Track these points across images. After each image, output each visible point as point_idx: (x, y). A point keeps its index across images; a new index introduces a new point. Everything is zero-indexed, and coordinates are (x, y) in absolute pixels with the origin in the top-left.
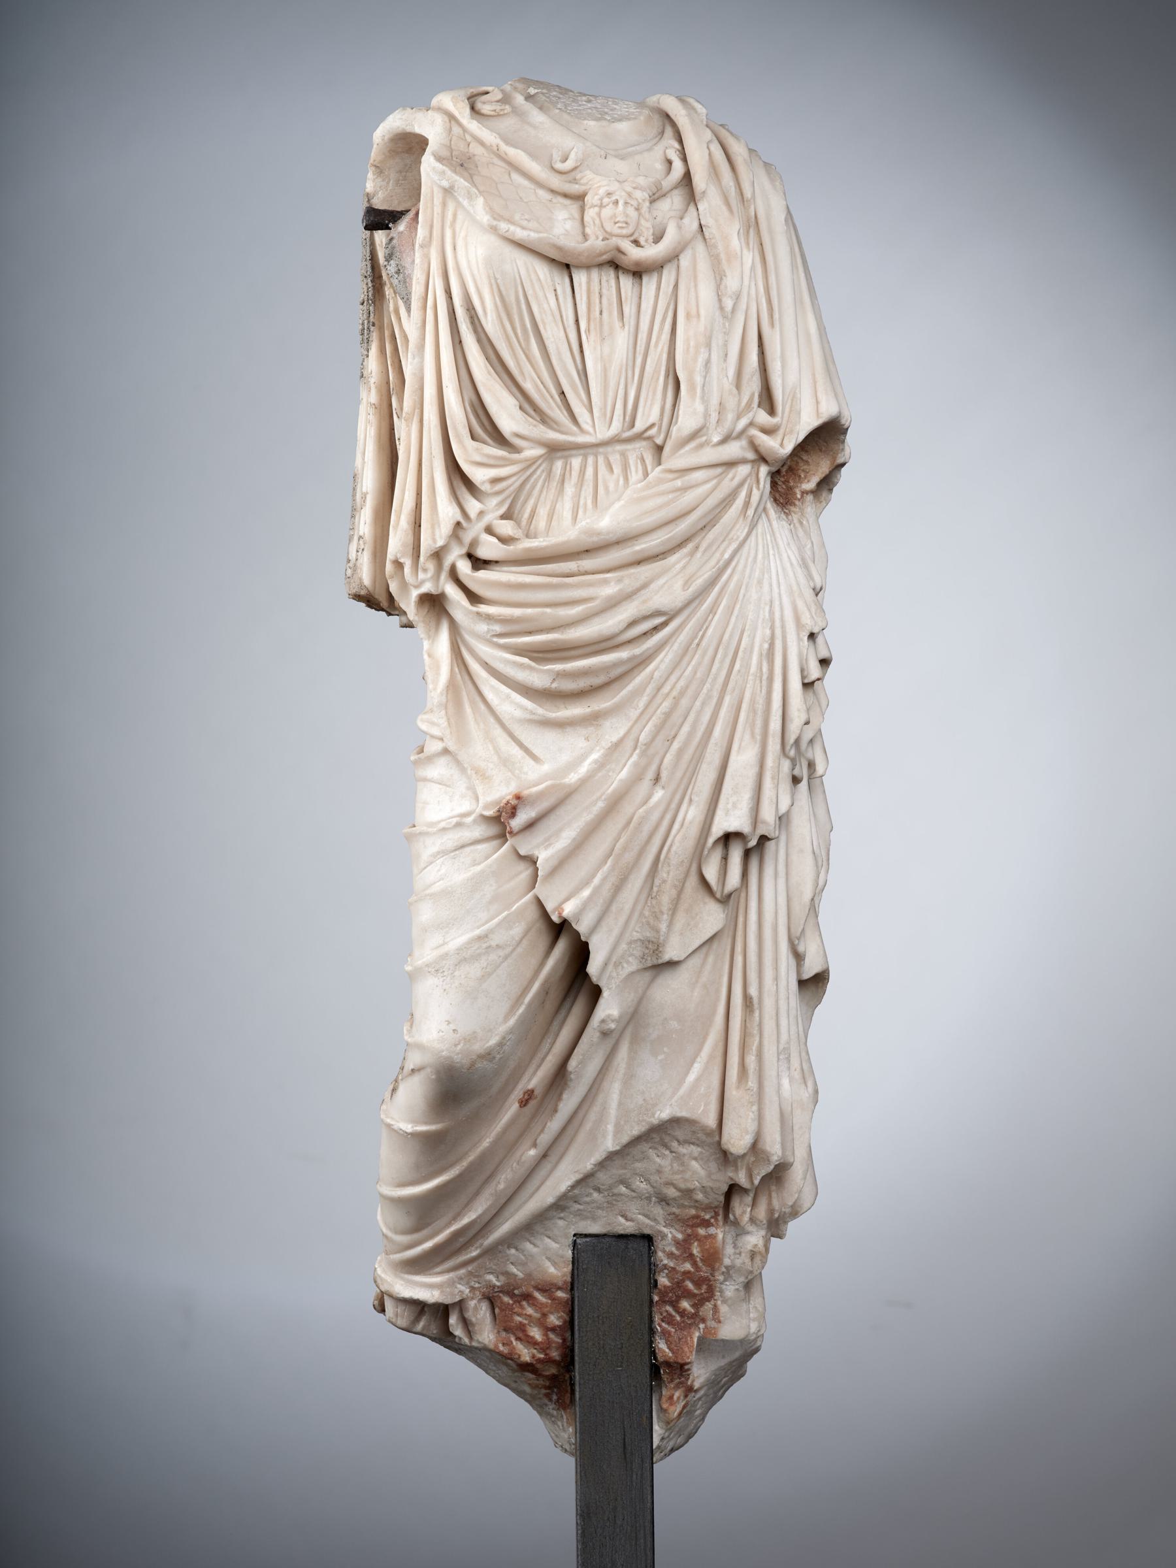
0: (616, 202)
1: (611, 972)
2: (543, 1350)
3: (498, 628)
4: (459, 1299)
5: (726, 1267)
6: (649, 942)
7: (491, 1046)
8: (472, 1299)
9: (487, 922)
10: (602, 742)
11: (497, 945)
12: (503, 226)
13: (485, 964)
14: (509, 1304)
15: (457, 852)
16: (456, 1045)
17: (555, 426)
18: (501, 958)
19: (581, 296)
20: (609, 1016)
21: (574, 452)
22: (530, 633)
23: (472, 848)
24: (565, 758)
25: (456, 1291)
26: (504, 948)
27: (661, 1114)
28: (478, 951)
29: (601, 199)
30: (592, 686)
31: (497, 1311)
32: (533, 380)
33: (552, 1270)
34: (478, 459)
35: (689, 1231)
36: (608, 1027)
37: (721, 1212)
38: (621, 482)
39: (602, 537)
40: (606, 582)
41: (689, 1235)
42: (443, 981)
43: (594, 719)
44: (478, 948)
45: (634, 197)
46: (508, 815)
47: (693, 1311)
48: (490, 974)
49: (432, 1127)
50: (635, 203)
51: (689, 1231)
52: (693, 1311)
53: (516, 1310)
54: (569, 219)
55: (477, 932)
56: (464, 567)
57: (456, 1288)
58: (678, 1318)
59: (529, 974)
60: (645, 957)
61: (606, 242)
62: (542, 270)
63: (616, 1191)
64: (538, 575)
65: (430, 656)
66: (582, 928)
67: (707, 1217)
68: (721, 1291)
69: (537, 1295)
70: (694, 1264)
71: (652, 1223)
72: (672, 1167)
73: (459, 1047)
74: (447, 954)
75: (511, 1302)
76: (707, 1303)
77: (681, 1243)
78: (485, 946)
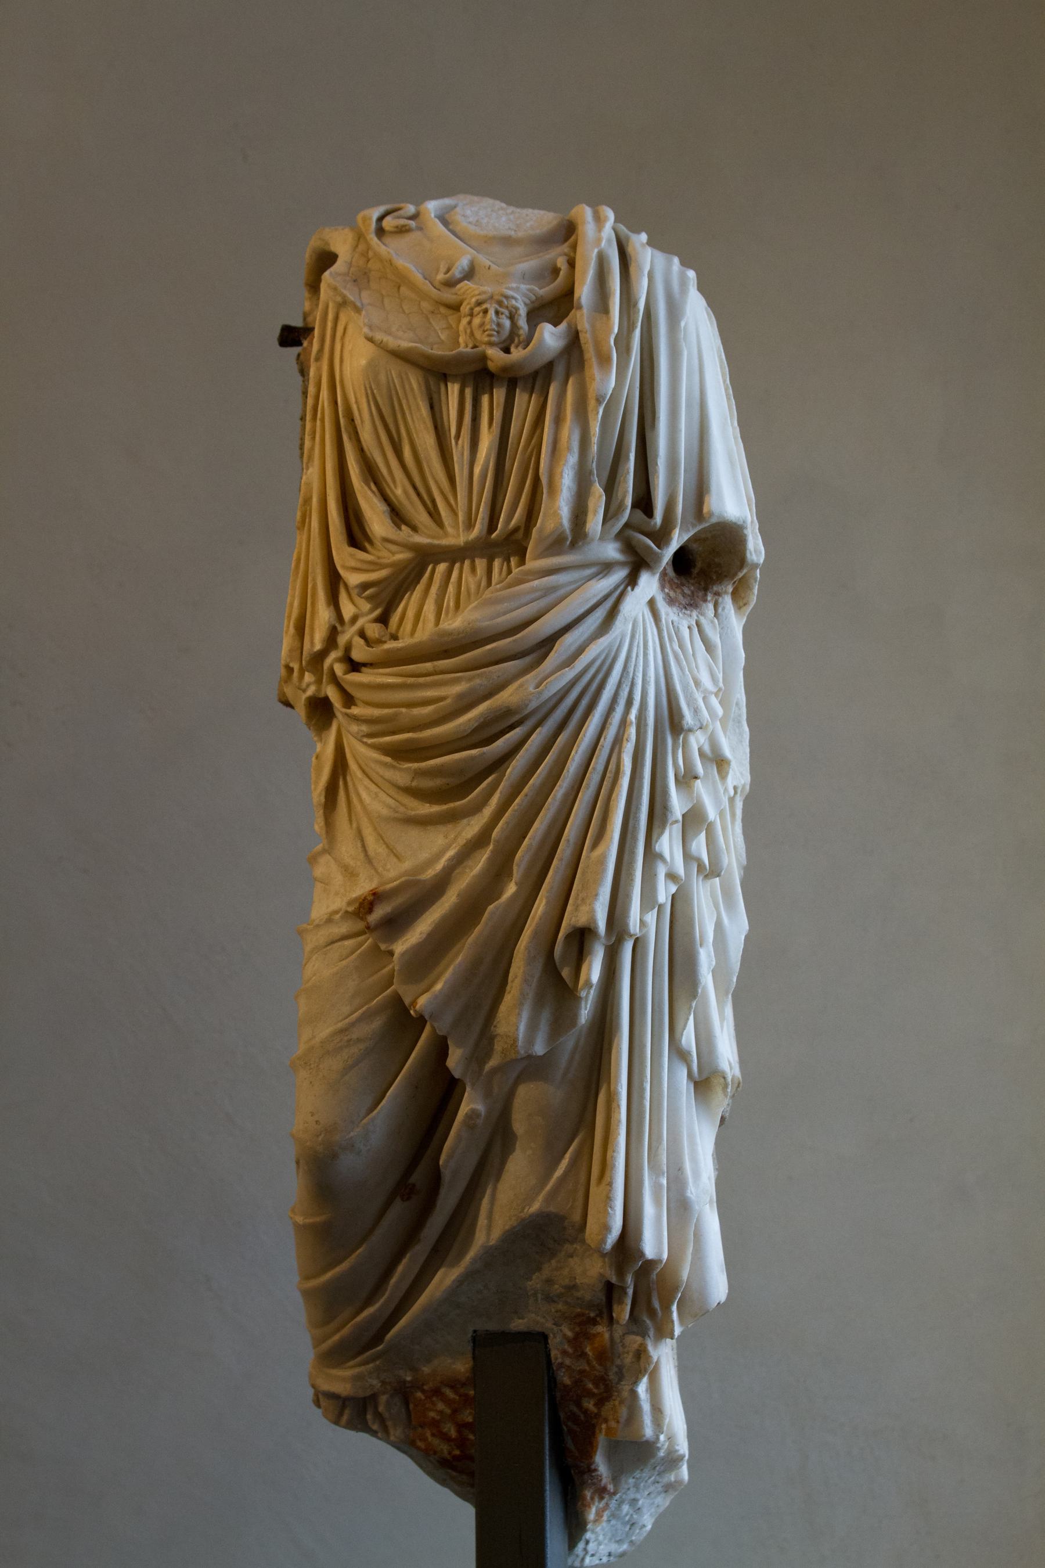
0: (486, 311)
3: (365, 728)
4: (370, 1393)
5: (617, 1366)
8: (384, 1393)
9: (349, 1015)
10: (459, 839)
11: (358, 1039)
12: (379, 336)
13: (346, 1057)
14: (421, 1400)
15: (328, 948)
16: (318, 1136)
19: (453, 402)
22: (394, 733)
23: (340, 943)
24: (424, 855)
29: (472, 309)
30: (448, 784)
31: (411, 1406)
34: (353, 564)
35: (577, 1329)
37: (605, 1310)
38: (484, 583)
40: (456, 681)
42: (310, 1074)
47: (595, 1411)
49: (318, 1219)
51: (577, 1329)
52: (595, 1411)
53: (427, 1406)
55: (340, 1025)
56: (339, 669)
61: (475, 350)
65: (317, 758)
67: (592, 1315)
70: (589, 1363)
73: (320, 1139)
74: (313, 1047)
78: (346, 1038)
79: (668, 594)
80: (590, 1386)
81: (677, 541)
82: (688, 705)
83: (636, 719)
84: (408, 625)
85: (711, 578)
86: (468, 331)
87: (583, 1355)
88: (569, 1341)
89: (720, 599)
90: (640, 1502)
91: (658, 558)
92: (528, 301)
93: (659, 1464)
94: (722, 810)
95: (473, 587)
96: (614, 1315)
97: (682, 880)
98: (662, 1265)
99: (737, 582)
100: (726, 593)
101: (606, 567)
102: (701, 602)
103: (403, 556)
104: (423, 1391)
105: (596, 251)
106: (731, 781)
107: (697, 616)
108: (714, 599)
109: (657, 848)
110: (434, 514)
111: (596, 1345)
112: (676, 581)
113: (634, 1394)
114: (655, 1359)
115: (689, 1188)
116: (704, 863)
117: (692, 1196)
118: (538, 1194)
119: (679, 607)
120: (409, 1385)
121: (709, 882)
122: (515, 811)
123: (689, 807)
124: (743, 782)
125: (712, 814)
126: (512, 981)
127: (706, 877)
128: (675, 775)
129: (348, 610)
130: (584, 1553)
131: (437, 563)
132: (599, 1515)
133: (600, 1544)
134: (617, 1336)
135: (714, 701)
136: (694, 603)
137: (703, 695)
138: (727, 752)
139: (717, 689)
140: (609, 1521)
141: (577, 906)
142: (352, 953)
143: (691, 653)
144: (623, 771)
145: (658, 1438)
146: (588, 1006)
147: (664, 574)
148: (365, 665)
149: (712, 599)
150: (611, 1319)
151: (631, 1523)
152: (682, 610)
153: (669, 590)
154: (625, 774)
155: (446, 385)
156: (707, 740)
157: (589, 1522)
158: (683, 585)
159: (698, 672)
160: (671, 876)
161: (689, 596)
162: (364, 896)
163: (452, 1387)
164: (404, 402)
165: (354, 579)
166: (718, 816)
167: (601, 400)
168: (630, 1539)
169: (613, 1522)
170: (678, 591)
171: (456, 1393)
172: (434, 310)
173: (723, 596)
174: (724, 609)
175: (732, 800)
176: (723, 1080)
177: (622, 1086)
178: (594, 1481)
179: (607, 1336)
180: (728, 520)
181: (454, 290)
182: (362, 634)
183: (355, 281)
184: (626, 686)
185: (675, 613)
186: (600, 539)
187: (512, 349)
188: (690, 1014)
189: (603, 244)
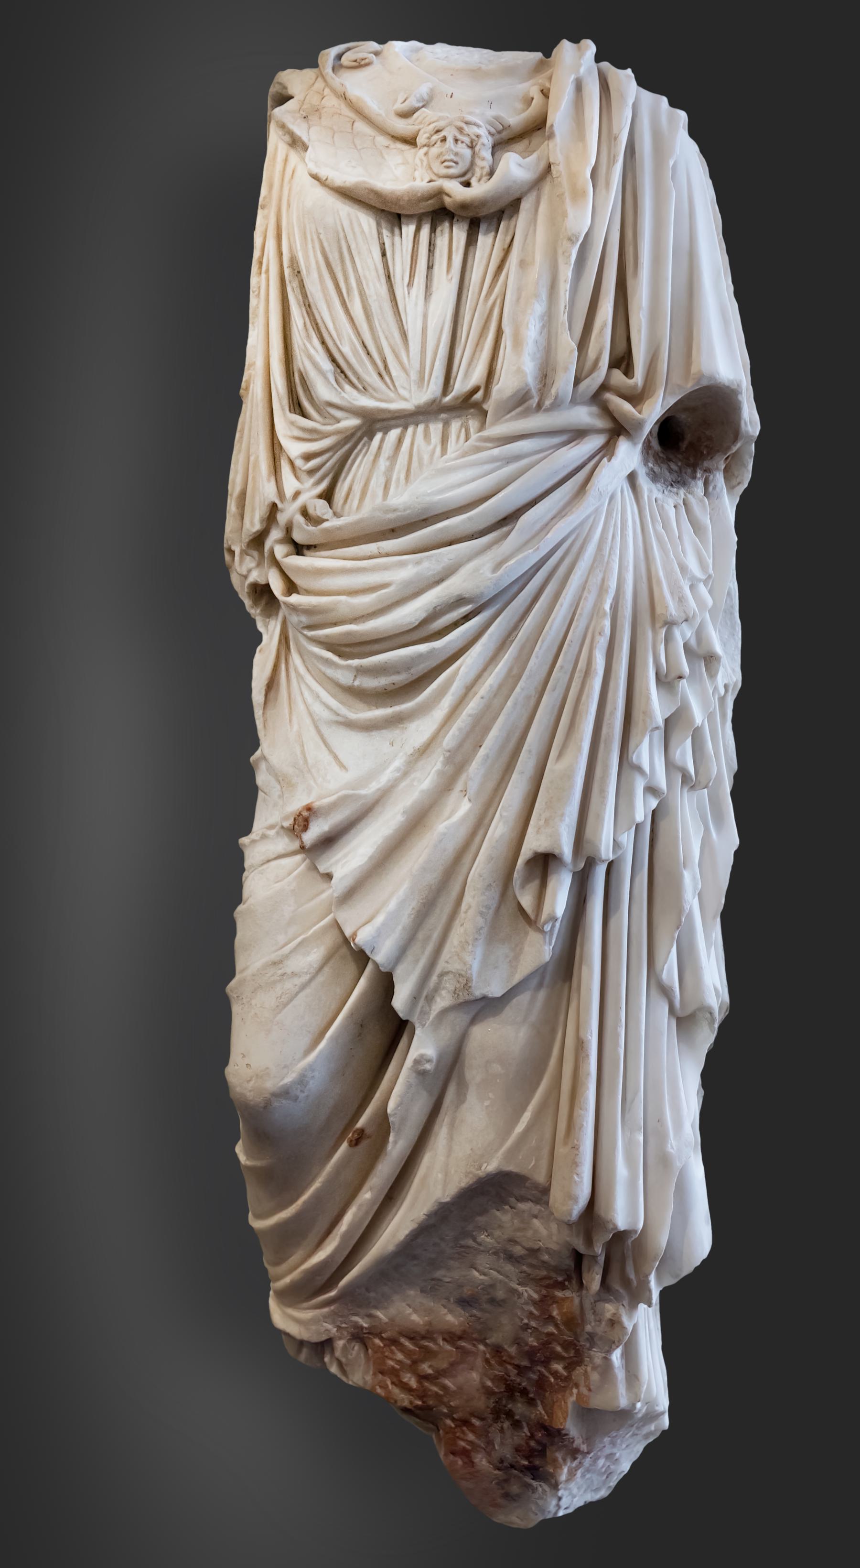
0: (444, 140)
1: (422, 1007)
2: (421, 1398)
3: (304, 619)
5: (589, 1333)
6: (459, 975)
7: (286, 1084)
8: (340, 1338)
17: (375, 394)
18: (297, 987)
20: (422, 1056)
21: (393, 422)
25: (322, 1329)
26: (300, 977)
27: (488, 1167)
28: (272, 979)
32: (352, 343)
33: (415, 1317)
35: (544, 1292)
36: (423, 1068)
37: (574, 1275)
39: (399, 514)
40: (402, 564)
41: (545, 1296)
43: (397, 721)
44: (273, 975)
45: (465, 133)
46: (301, 828)
47: (565, 1374)
48: (285, 1005)
50: (467, 140)
51: (544, 1292)
52: (565, 1374)
54: (403, 164)
56: (280, 551)
57: (322, 1326)
58: (552, 1380)
59: (334, 1006)
60: (457, 992)
61: (432, 184)
62: (366, 222)
63: (463, 1243)
64: (344, 559)
66: (381, 956)
67: (560, 1279)
68: (590, 1357)
69: (403, 1340)
70: (557, 1326)
71: (507, 1280)
72: (513, 1222)
75: (382, 1345)
76: (578, 1368)
77: (538, 1303)
78: (280, 972)
79: (652, 470)
80: (559, 1349)
81: (662, 405)
82: (672, 594)
83: (610, 609)
84: (355, 501)
85: (702, 453)
86: (425, 163)
87: (550, 1319)
88: (535, 1303)
89: (711, 477)
90: (618, 1455)
91: (640, 425)
92: (493, 130)
93: (636, 1423)
94: (711, 712)
95: (426, 457)
96: (584, 1282)
97: (664, 794)
98: (637, 1235)
99: (730, 458)
100: (717, 469)
101: (578, 434)
102: (690, 480)
103: (352, 422)
104: (382, 1339)
105: (573, 77)
106: (721, 679)
107: (685, 495)
108: (705, 476)
109: (634, 759)
110: (384, 372)
111: (565, 1310)
112: (661, 455)
113: (607, 1360)
114: (630, 1329)
115: (670, 1141)
116: (689, 773)
117: (672, 1151)
118: (497, 1150)
119: (664, 483)
120: (365, 1331)
121: (695, 794)
122: (470, 715)
123: (673, 711)
124: (735, 680)
125: (699, 717)
126: (466, 912)
127: (693, 788)
128: (657, 674)
129: (290, 483)
130: (556, 1508)
131: (386, 431)
132: (572, 1474)
133: (574, 1497)
134: (587, 1305)
135: (703, 589)
136: (681, 479)
137: (690, 584)
138: (718, 649)
139: (706, 577)
140: (583, 1476)
141: (539, 829)
142: (289, 874)
143: (677, 535)
144: (595, 669)
145: (634, 1405)
146: (553, 942)
147: (647, 446)
148: (309, 547)
149: (702, 476)
150: (581, 1285)
151: (608, 1473)
152: (667, 487)
153: (654, 465)
154: (597, 673)
155: (401, 229)
156: (694, 634)
157: (561, 1483)
158: (670, 460)
159: (685, 556)
160: (651, 790)
161: (676, 472)
162: (298, 812)
163: (411, 1339)
164: (353, 246)
165: (294, 449)
166: (706, 720)
167: (574, 239)
168: (608, 1486)
169: (588, 1476)
170: (664, 467)
171: (416, 1345)
172: (389, 145)
173: (714, 472)
174: (714, 488)
175: (722, 700)
176: (709, 1015)
177: (591, 1033)
178: (565, 1443)
179: (577, 1301)
180: (720, 383)
181: (410, 121)
182: (305, 512)
183: (305, 118)
184: (600, 571)
185: (659, 490)
186: (571, 401)
187: (474, 181)
188: (672, 946)
189: (582, 70)
